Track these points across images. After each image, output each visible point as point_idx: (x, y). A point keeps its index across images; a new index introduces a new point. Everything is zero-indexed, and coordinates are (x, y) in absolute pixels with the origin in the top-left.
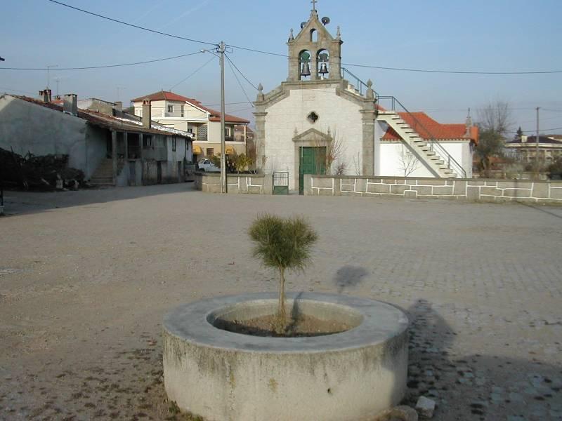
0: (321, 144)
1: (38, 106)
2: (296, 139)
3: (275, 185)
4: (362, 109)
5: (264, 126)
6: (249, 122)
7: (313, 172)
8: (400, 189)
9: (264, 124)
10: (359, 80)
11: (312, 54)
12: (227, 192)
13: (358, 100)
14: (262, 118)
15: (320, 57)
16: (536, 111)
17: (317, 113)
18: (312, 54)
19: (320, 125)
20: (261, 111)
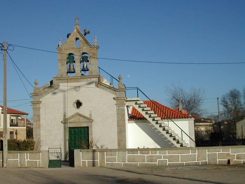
0: (85, 125)
1: (195, 166)
2: (65, 122)
3: (50, 159)
4: (115, 97)
5: (39, 112)
6: (28, 114)
7: (80, 147)
8: (154, 158)
9: (39, 110)
10: (111, 76)
11: (77, 58)
12: (3, 167)
13: (111, 88)
14: (38, 106)
15: (85, 59)
16: (217, 99)
17: (81, 101)
18: (77, 58)
19: (82, 110)
20: (37, 100)
